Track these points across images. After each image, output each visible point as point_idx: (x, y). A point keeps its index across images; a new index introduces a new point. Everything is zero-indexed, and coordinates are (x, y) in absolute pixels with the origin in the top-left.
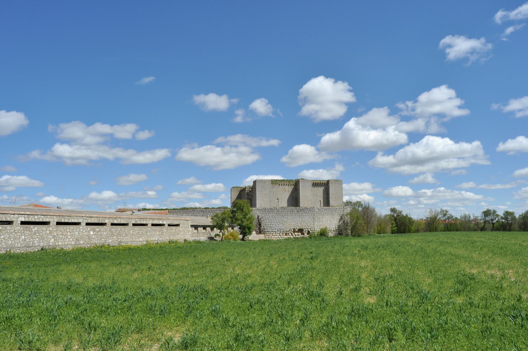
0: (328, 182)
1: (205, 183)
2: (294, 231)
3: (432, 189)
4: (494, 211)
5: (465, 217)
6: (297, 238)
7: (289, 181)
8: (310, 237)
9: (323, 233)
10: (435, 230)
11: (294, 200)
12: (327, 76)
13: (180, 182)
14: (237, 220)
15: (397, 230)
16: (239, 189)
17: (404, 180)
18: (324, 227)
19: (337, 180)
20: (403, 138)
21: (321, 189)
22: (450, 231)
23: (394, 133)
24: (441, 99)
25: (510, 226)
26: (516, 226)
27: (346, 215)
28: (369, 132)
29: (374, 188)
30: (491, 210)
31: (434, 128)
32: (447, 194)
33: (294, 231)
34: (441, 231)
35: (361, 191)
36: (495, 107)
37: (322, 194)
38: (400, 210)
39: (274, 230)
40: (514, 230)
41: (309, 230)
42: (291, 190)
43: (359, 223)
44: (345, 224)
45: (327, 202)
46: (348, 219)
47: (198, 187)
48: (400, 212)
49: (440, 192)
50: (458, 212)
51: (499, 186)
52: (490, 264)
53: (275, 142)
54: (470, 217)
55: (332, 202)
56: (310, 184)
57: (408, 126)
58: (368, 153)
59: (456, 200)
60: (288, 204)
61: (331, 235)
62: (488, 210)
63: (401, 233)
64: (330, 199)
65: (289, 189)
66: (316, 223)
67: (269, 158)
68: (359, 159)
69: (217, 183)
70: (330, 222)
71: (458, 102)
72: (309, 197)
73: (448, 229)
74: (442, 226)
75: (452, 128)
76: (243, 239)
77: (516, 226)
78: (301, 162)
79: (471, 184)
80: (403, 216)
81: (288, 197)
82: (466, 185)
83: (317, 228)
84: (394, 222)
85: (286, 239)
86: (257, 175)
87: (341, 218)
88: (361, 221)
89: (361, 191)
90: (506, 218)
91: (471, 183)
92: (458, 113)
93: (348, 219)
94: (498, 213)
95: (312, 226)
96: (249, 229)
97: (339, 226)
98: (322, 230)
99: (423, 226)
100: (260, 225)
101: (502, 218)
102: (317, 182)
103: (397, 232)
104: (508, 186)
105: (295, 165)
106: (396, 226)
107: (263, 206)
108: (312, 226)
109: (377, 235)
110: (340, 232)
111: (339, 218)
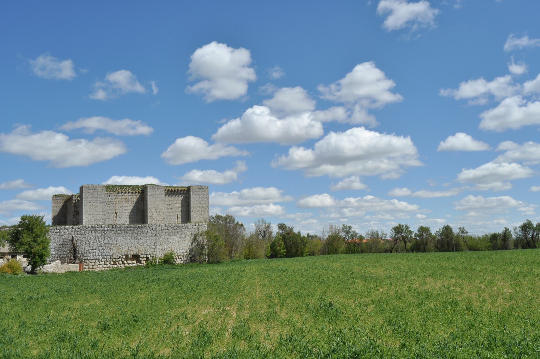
0: (189, 188)
1: (35, 187)
2: (127, 258)
3: (373, 196)
4: (406, 226)
5: (372, 234)
6: (129, 268)
7: (134, 187)
8: (147, 266)
9: (168, 261)
10: (336, 252)
11: (140, 215)
12: (219, 41)
13: (273, 165)
14: (22, 244)
15: (286, 252)
16: (64, 198)
17: (324, 184)
18: (170, 252)
19: (201, 187)
20: (317, 129)
21: (179, 199)
22: (354, 252)
23: (306, 122)
24: (368, 79)
25: (425, 245)
26: (431, 245)
27: (201, 235)
28: (284, 118)
29: (283, 195)
30: (403, 226)
31: (359, 116)
32: (374, 204)
33: (127, 258)
34: (342, 253)
35: (267, 200)
36: (444, 93)
37: (180, 206)
38: (290, 227)
39: (98, 257)
40: (430, 251)
41: (149, 256)
42: (135, 200)
43: (221, 244)
44: (200, 246)
45: (186, 217)
46: (204, 240)
47: (30, 193)
48: (291, 229)
49: (366, 201)
50: (362, 230)
51: (438, 194)
52: (492, 290)
53: (144, 130)
54: (378, 234)
55: (193, 216)
56: (163, 192)
57: (324, 116)
58: (280, 147)
59: (387, 211)
60: (130, 219)
61: (179, 262)
62: (400, 225)
63: (291, 256)
64: (192, 213)
65: (133, 199)
66: (158, 246)
67: (139, 152)
68: (263, 158)
69: (56, 186)
70: (179, 245)
71: (389, 84)
72: (160, 210)
73: (350, 249)
74: (343, 247)
75: (384, 119)
76: (32, 272)
77: (431, 245)
78: (188, 159)
79: (404, 192)
80: (294, 234)
81: (131, 209)
82: (399, 192)
83: (159, 252)
84: (283, 243)
85: (113, 270)
86: (202, 171)
87: (195, 239)
88: (221, 242)
89: (267, 200)
90: (421, 235)
91: (405, 189)
92: (388, 97)
93: (204, 240)
94: (411, 229)
95: (153, 250)
96: (41, 256)
97: (191, 250)
98: (166, 255)
99: (319, 247)
100: (75, 250)
101: (416, 235)
102: (173, 189)
103: (287, 256)
104: (447, 194)
105: (179, 162)
106: (286, 248)
107: (93, 223)
108: (153, 250)
109: (243, 260)
110: (193, 259)
111: (192, 238)
